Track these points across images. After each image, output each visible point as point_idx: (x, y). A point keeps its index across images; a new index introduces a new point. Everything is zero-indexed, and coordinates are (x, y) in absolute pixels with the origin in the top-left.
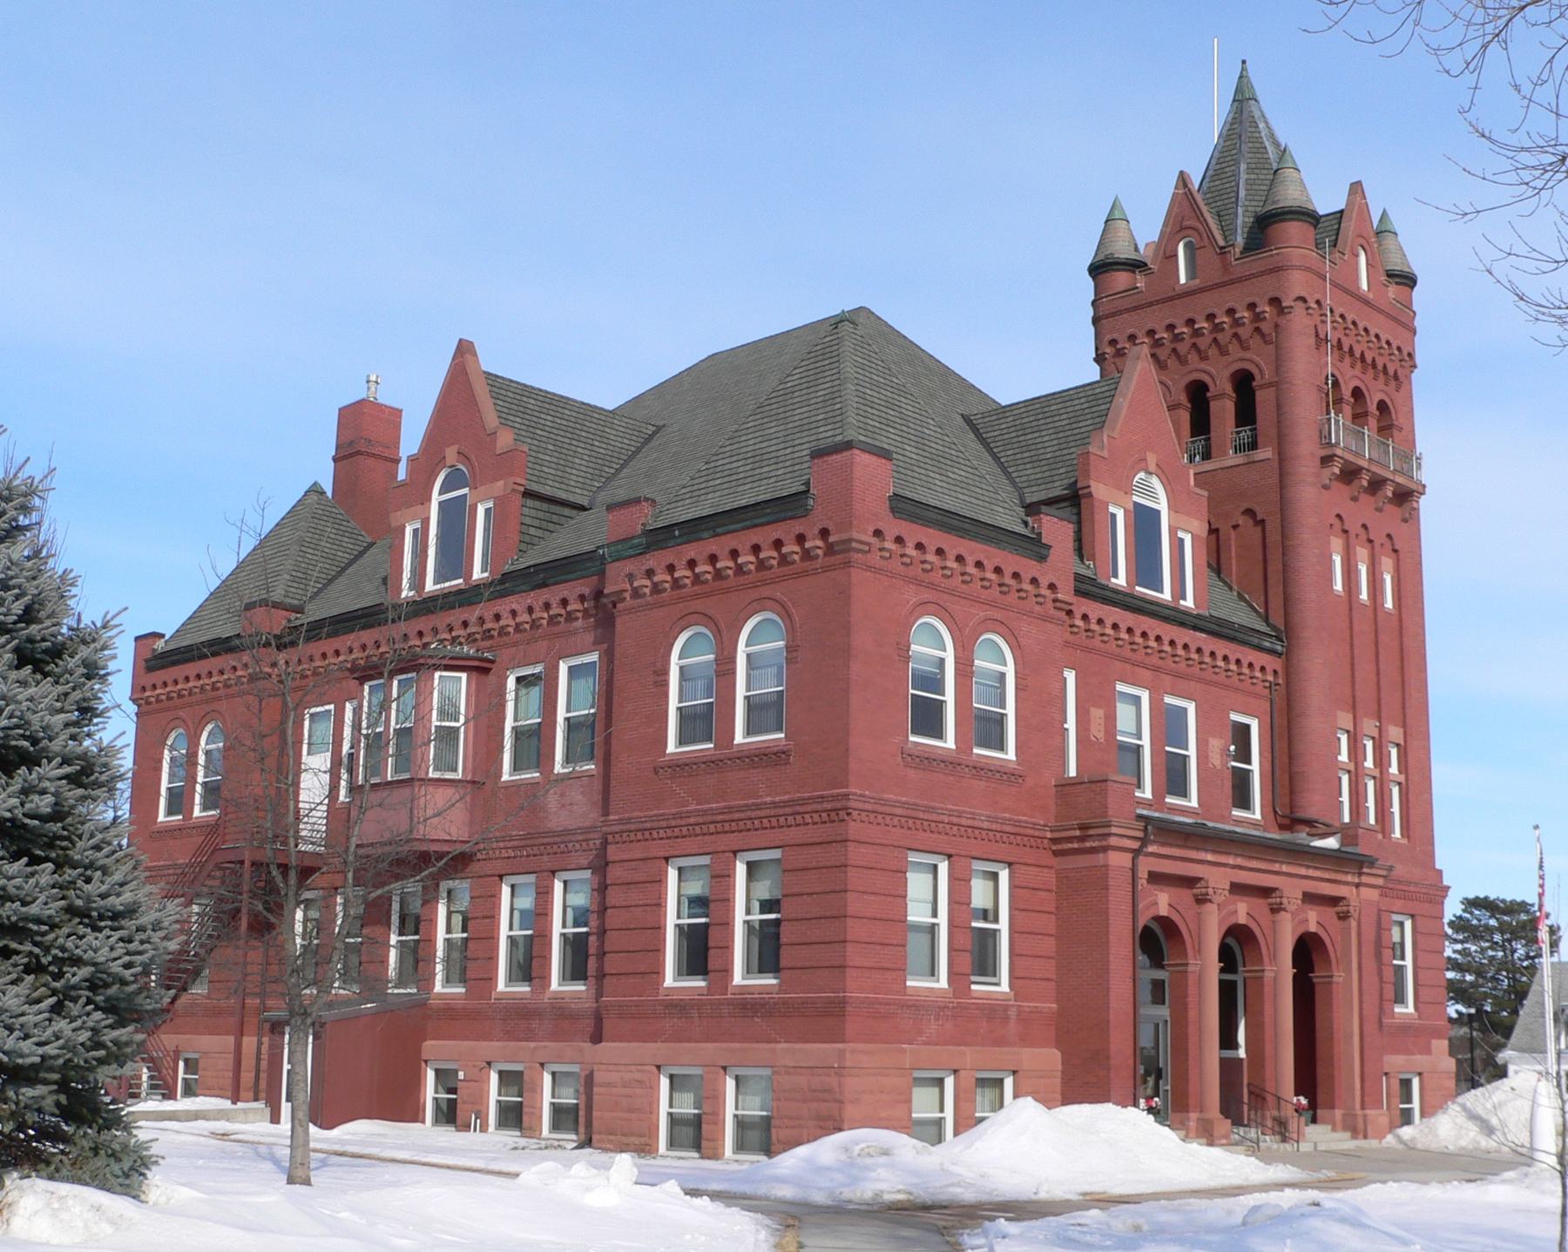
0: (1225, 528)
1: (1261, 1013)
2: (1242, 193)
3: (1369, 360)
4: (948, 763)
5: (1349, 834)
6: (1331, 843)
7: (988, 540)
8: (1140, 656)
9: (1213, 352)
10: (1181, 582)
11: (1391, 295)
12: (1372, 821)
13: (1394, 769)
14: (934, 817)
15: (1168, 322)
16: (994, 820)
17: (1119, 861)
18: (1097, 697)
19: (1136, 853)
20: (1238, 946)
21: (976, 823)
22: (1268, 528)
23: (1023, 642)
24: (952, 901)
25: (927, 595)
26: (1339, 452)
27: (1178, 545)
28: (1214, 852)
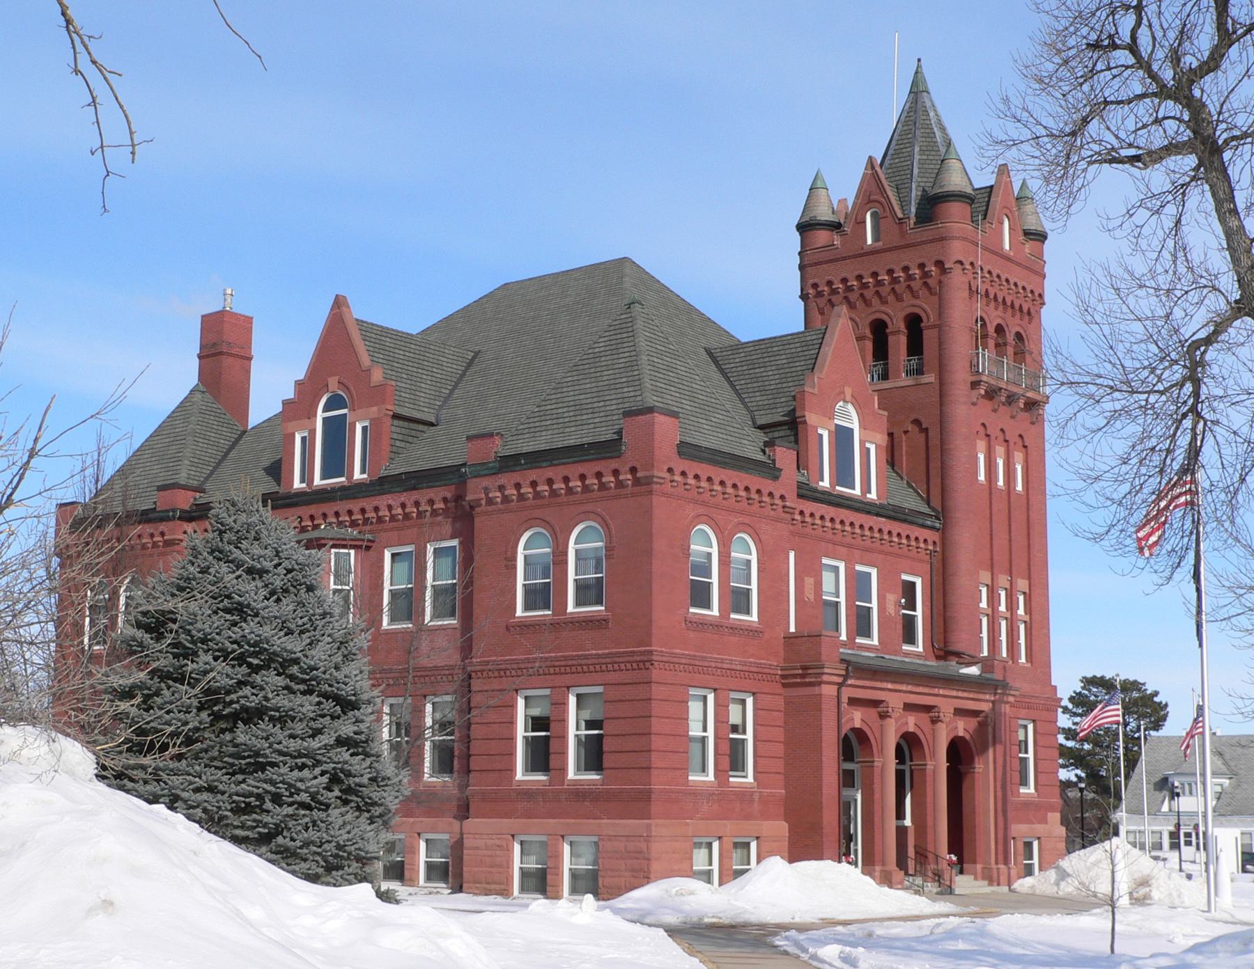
0: (898, 433)
1: (924, 795)
2: (916, 171)
3: (1009, 303)
4: (715, 626)
5: (987, 665)
6: (974, 670)
7: (740, 469)
8: (839, 538)
9: (891, 298)
10: (869, 481)
11: (1027, 251)
12: (1004, 655)
13: (1021, 611)
14: (706, 664)
15: (857, 273)
16: (745, 664)
17: (828, 691)
18: (810, 569)
19: (840, 685)
20: (909, 746)
21: (733, 667)
22: (930, 435)
23: (763, 537)
24: (717, 721)
25: (701, 510)
26: (984, 378)
27: (865, 453)
28: (893, 682)
